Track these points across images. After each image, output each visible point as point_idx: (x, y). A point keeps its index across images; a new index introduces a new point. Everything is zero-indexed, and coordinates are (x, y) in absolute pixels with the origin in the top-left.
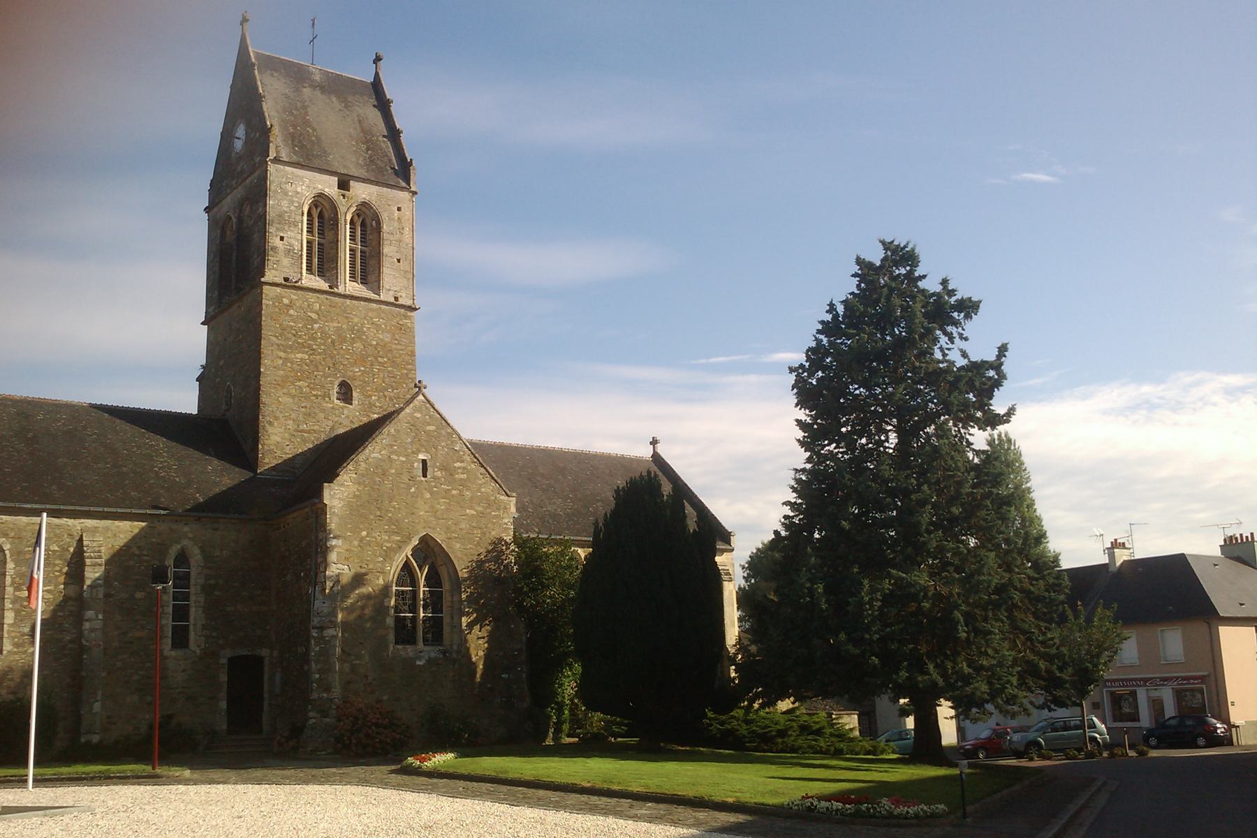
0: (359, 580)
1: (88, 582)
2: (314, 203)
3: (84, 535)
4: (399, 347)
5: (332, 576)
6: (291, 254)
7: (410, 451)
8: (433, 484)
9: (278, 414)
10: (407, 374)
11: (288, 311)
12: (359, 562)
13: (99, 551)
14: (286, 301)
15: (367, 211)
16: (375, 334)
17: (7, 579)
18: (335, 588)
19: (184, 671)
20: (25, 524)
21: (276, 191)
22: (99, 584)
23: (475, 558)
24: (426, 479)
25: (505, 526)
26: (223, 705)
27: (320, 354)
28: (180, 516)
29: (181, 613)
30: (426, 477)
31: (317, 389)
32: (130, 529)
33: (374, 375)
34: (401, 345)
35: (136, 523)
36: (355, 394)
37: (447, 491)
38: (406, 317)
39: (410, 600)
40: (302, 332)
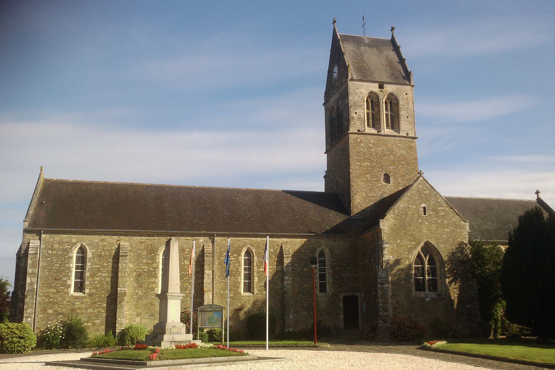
0: (397, 262)
1: (285, 265)
2: (388, 98)
3: (283, 245)
4: (410, 156)
6: (360, 119)
7: (417, 203)
9: (358, 190)
10: (414, 168)
13: (289, 252)
14: (359, 140)
18: (387, 266)
20: (260, 241)
21: (352, 93)
23: (451, 251)
27: (375, 162)
30: (426, 215)
32: (300, 242)
34: (411, 155)
35: (303, 239)
36: (391, 179)
37: (435, 221)
38: (412, 142)
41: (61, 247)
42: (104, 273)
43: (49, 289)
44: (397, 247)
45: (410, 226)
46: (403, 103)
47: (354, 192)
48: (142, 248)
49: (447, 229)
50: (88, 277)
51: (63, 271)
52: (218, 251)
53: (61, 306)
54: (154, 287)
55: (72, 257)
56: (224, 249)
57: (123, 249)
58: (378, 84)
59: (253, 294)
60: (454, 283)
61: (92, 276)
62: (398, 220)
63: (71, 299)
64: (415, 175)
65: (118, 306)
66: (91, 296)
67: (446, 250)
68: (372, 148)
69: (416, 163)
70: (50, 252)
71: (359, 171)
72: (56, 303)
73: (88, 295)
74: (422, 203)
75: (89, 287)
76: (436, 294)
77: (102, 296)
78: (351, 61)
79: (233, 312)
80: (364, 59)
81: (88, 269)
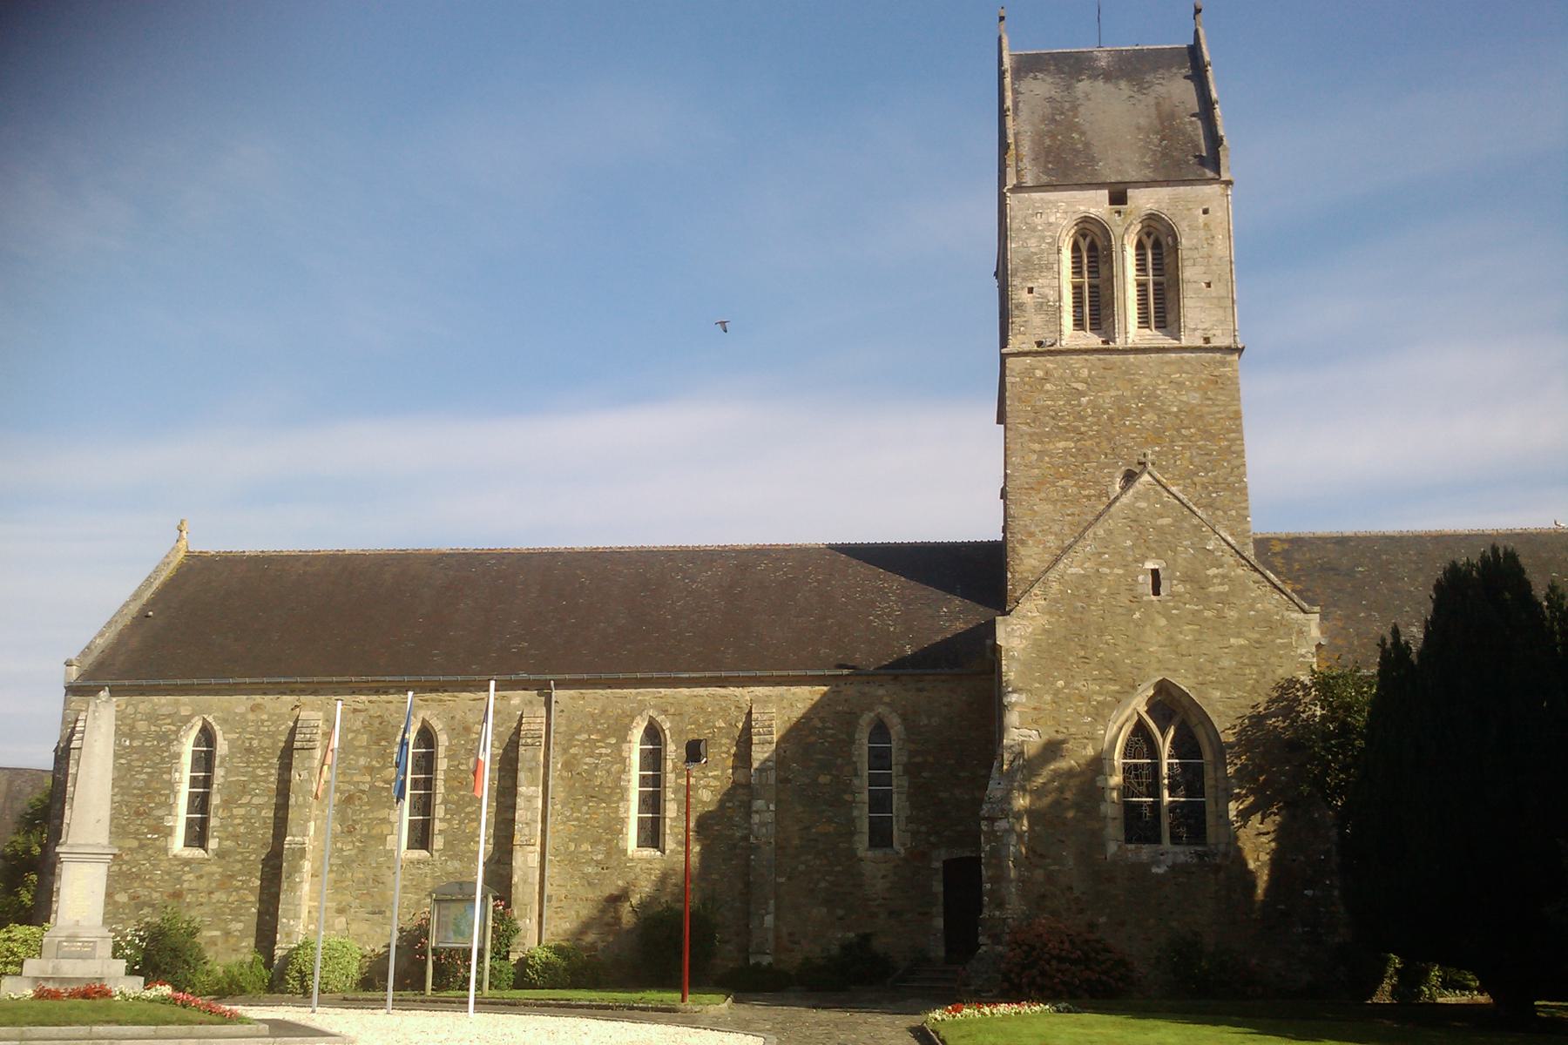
0: (1052, 749)
1: (756, 765)
2: (1081, 232)
3: (754, 706)
4: (1216, 409)
5: (1012, 746)
6: (1045, 308)
7: (1130, 559)
8: (1171, 604)
9: (1033, 529)
10: (1230, 447)
11: (1043, 387)
13: (770, 726)
14: (1039, 373)
15: (1158, 226)
16: (1175, 397)
17: (668, 764)
18: (1016, 763)
19: (884, 877)
20: (686, 697)
21: (1020, 229)
22: (769, 766)
23: (1248, 712)
25: (1301, 659)
26: (939, 923)
27: (1091, 438)
28: (872, 675)
29: (880, 802)
30: (1159, 594)
31: (1089, 487)
32: (809, 696)
33: (1175, 456)
34: (1217, 405)
35: (817, 688)
37: (1194, 613)
38: (1223, 364)
39: (1143, 777)
40: (1064, 411)
41: (153, 728)
42: (257, 795)
43: (122, 838)
44: (1055, 702)
45: (1101, 632)
47: (1019, 536)
48: (358, 724)
49: (1238, 637)
50: (217, 807)
51: (157, 791)
52: (562, 729)
53: (147, 883)
54: (385, 832)
55: (178, 756)
56: (580, 724)
57: (304, 730)
58: (1106, 192)
59: (663, 852)
60: (1259, 816)
61: (227, 804)
62: (1061, 617)
63: (173, 865)
64: (1232, 469)
65: (284, 886)
66: (224, 858)
68: (1082, 394)
69: (1239, 430)
70: (128, 743)
71: (1036, 471)
72: (138, 876)
73: (216, 855)
74: (1147, 557)
75: (220, 835)
76: (1196, 852)
77: (252, 858)
78: (1032, 132)
79: (601, 906)
80: (1077, 120)
81: (218, 785)
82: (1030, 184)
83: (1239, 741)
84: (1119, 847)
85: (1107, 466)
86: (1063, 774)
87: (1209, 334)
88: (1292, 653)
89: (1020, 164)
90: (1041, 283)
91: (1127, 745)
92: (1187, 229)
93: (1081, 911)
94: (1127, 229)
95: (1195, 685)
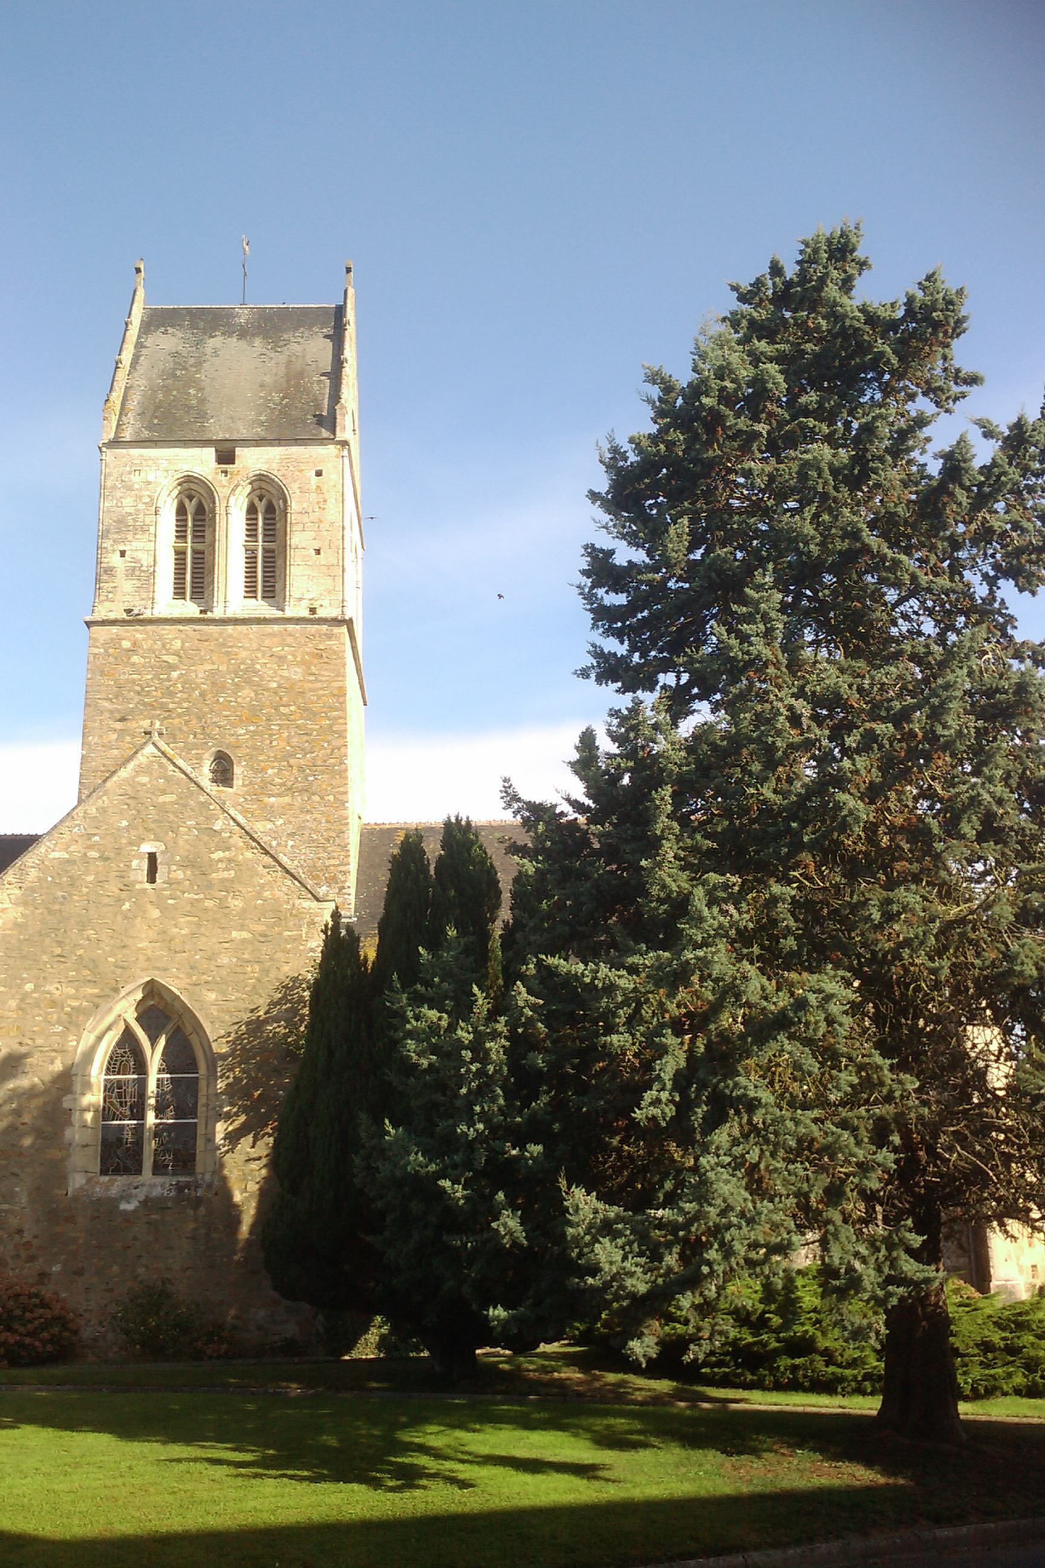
4: (319, 685)
6: (137, 573)
7: (124, 841)
10: (331, 726)
12: (16, 1036)
14: (126, 644)
15: (270, 489)
16: (275, 672)
21: (114, 487)
23: (246, 1016)
24: (153, 886)
27: (179, 716)
33: (271, 735)
36: (238, 770)
37: (193, 903)
38: (329, 637)
45: (83, 926)
46: (305, 505)
60: (250, 1138)
64: (333, 751)
67: (228, 1012)
68: (172, 667)
71: (116, 752)
82: (128, 439)
83: (234, 1050)
84: (89, 1181)
85: (195, 746)
86: (24, 1094)
87: (316, 605)
88: (301, 948)
89: (124, 418)
90: (137, 548)
91: (111, 1058)
92: (298, 491)
93: (32, 1258)
94: (233, 490)
95: (187, 986)
